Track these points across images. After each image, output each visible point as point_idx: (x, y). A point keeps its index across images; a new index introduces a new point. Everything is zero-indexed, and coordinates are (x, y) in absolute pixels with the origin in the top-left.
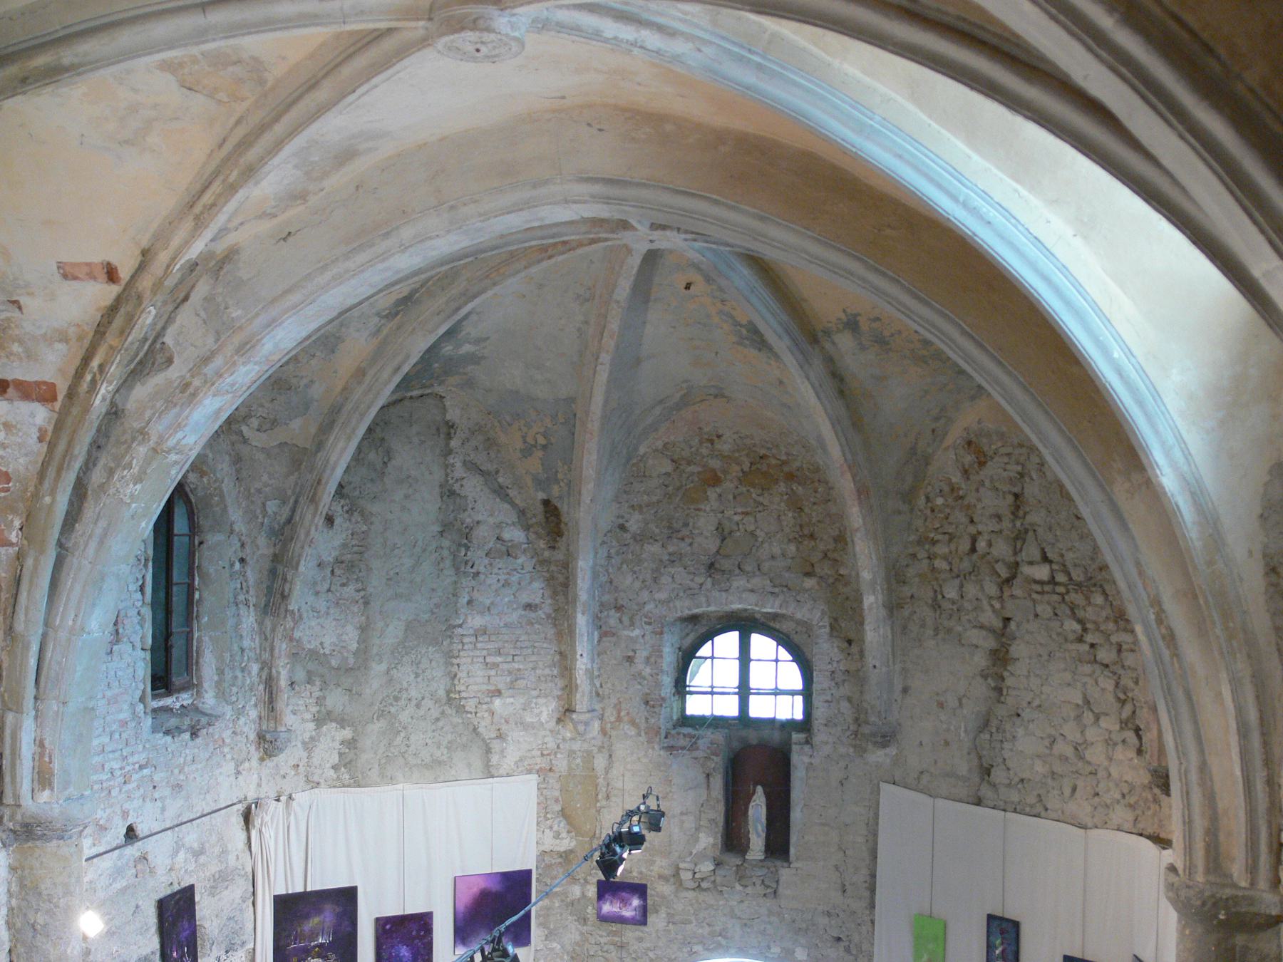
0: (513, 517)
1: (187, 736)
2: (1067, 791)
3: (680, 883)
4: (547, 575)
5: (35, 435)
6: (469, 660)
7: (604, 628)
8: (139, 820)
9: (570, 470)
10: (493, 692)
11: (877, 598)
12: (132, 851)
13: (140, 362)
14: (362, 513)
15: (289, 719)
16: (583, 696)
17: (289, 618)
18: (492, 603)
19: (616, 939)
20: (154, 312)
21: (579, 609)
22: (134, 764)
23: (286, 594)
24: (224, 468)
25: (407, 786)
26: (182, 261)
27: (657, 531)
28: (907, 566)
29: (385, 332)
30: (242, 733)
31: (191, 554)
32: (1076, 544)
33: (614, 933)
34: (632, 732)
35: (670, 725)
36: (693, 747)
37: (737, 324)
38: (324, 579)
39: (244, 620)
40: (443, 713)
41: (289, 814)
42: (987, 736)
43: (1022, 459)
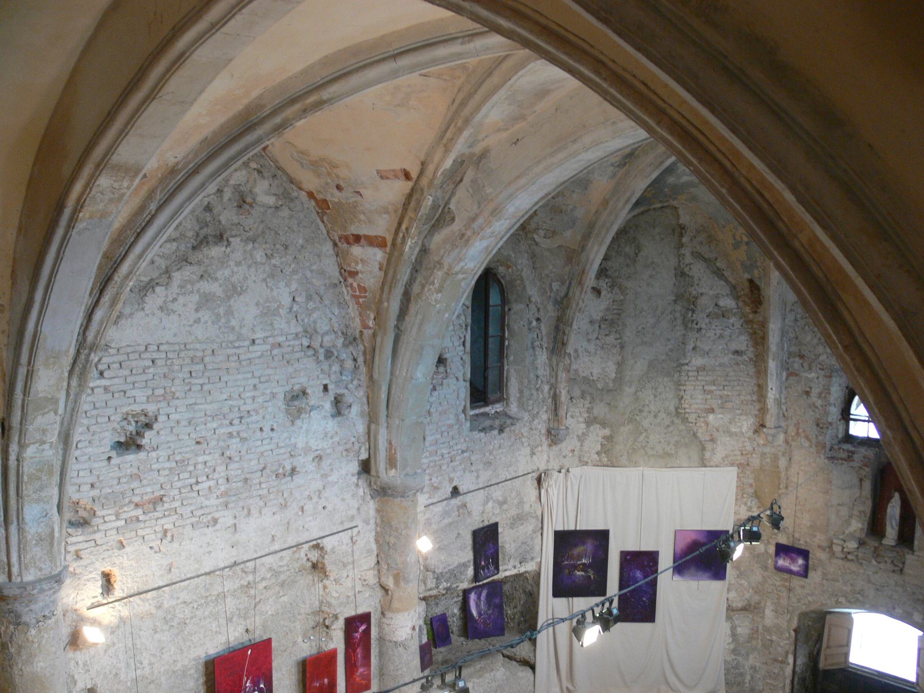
0: (727, 290)
1: (496, 432)
3: (832, 554)
4: (751, 331)
5: (377, 266)
6: (693, 388)
12: (456, 501)
13: (438, 220)
14: (620, 288)
15: (569, 422)
16: (772, 416)
18: (710, 349)
19: (787, 584)
20: (431, 198)
22: (457, 450)
23: (565, 342)
24: (523, 262)
25: (645, 469)
26: (441, 170)
30: (536, 429)
33: (786, 580)
35: (836, 441)
36: (849, 458)
39: (539, 357)
40: (672, 422)
41: (567, 481)
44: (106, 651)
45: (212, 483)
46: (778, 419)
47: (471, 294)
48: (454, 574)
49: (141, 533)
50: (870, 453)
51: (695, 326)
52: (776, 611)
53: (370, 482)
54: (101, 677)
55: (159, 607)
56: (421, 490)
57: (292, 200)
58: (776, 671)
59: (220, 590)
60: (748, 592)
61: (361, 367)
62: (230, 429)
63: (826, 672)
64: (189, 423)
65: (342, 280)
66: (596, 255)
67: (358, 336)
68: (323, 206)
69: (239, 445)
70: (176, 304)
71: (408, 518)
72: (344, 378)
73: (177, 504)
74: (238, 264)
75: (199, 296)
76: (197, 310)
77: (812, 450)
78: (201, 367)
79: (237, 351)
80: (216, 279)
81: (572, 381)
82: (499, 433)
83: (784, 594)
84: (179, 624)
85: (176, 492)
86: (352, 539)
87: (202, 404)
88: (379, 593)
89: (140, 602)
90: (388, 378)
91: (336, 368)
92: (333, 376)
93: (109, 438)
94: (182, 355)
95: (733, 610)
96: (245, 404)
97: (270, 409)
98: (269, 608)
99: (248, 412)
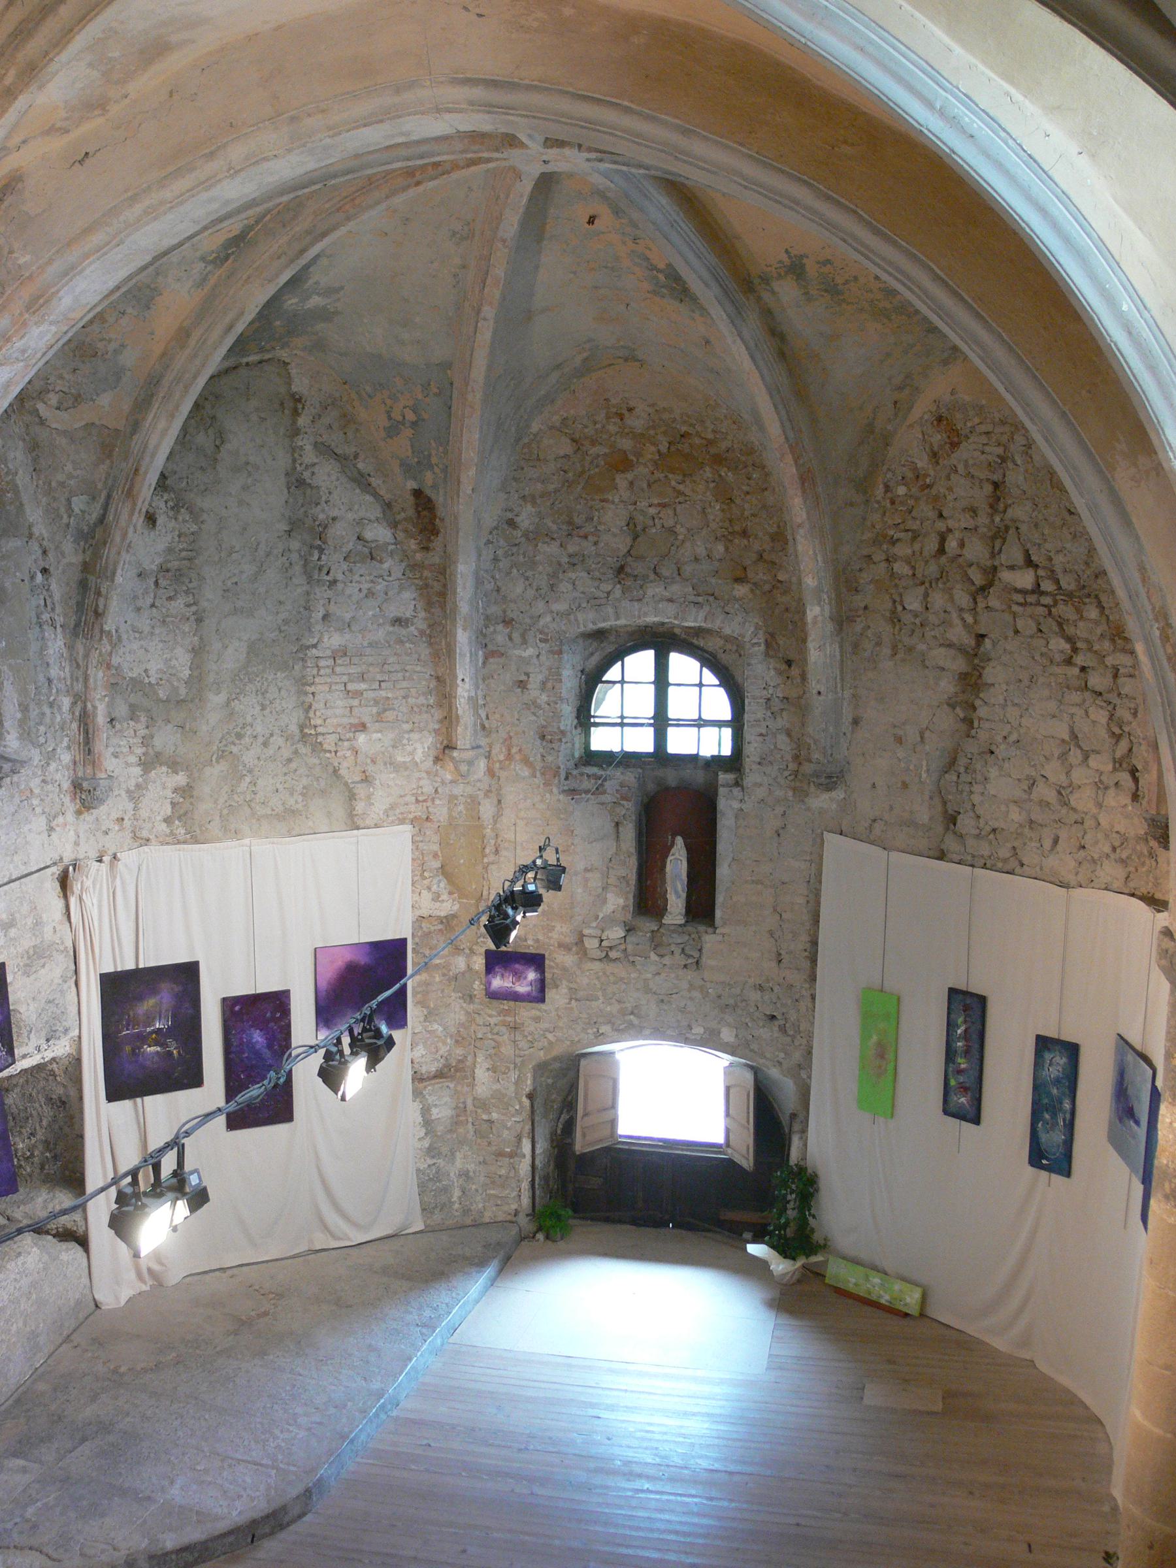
0: (376, 512)
2: (1048, 843)
3: (584, 953)
7: (490, 647)
9: (446, 452)
11: (823, 610)
15: (110, 764)
16: (466, 728)
18: (353, 617)
23: (100, 611)
25: (255, 841)
27: (554, 527)
28: (860, 570)
29: (212, 280)
30: (53, 781)
32: (1068, 546)
33: (506, 1012)
35: (571, 764)
36: (599, 790)
37: (653, 268)
38: (146, 592)
39: (50, 644)
40: (296, 752)
41: (114, 878)
42: (955, 778)
43: (1004, 439)
50: (630, 777)
52: (493, 1069)
58: (503, 1172)
60: (444, 1043)
95: (422, 1080)
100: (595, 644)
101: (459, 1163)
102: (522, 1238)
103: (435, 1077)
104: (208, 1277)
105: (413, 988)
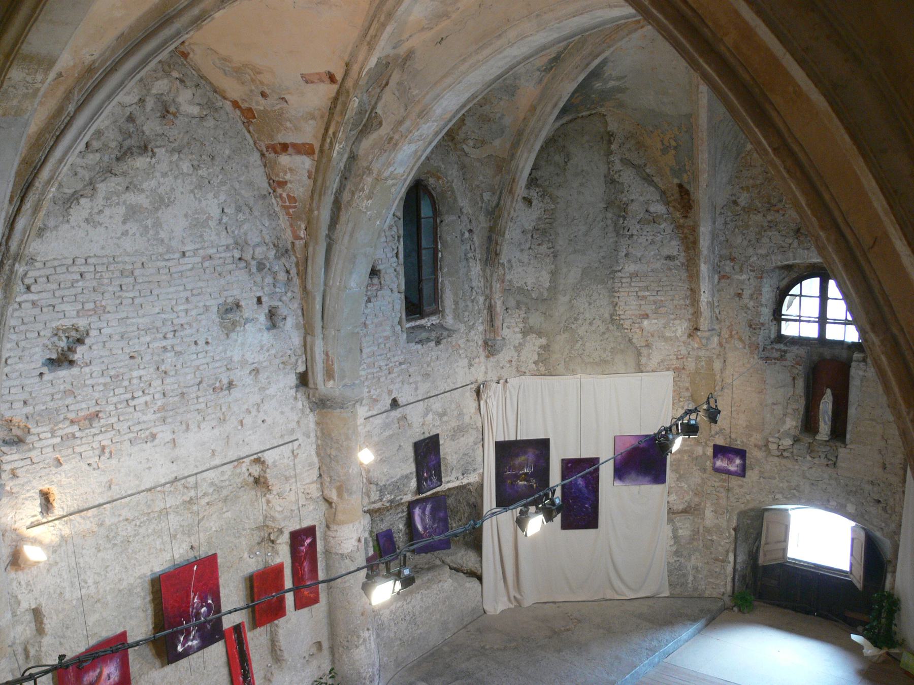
1: (433, 344)
5: (306, 175)
7: (722, 273)
8: (400, 395)
10: (643, 315)
12: (396, 413)
13: (364, 125)
14: (551, 197)
15: (506, 332)
17: (501, 268)
20: (357, 100)
21: (702, 260)
23: (498, 252)
24: (453, 173)
25: (583, 376)
26: (366, 70)
27: (760, 205)
29: (545, 80)
30: (473, 341)
31: (435, 228)
33: (724, 481)
34: (740, 345)
36: (782, 358)
38: (526, 241)
39: (473, 269)
40: (608, 328)
41: (505, 392)
44: (48, 570)
45: (148, 398)
46: (712, 321)
47: (402, 203)
48: (397, 486)
49: (78, 449)
51: (627, 233)
52: (715, 512)
53: (309, 395)
54: (46, 597)
55: (101, 525)
56: (360, 401)
57: (216, 110)
58: (717, 570)
59: (162, 506)
60: (688, 494)
61: (294, 279)
62: (164, 343)
63: (765, 568)
64: (122, 337)
65: (272, 191)
66: (525, 163)
67: (290, 247)
68: (248, 115)
69: (174, 360)
70: (102, 216)
71: (348, 429)
72: (277, 290)
73: (114, 420)
74: (164, 175)
75: (126, 208)
76: (124, 222)
77: (746, 351)
78: (131, 280)
79: (169, 264)
80: (143, 191)
81: (506, 291)
82: (436, 345)
83: (723, 494)
84: (122, 542)
85: (112, 407)
86: (293, 452)
87: (134, 318)
88: (324, 506)
89: (82, 521)
90: (322, 289)
91: (269, 280)
92: (266, 289)
93: (39, 355)
94: (111, 268)
95: (674, 513)
96: (178, 317)
97: (204, 322)
98: (213, 524)
99: (182, 325)
100: (786, 273)
101: (693, 561)
102: (725, 608)
103: (682, 512)
104: (546, 606)
105: (671, 462)
